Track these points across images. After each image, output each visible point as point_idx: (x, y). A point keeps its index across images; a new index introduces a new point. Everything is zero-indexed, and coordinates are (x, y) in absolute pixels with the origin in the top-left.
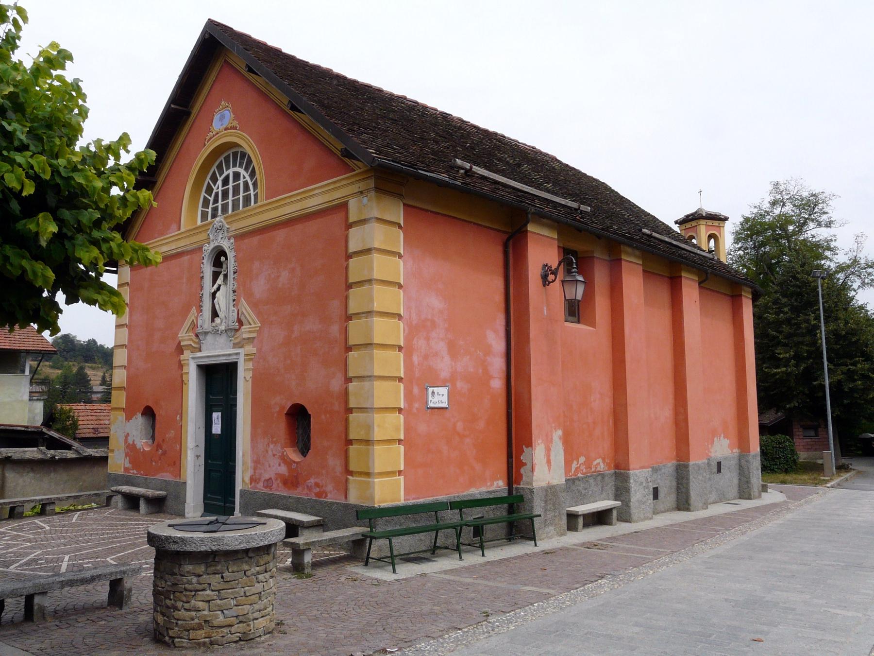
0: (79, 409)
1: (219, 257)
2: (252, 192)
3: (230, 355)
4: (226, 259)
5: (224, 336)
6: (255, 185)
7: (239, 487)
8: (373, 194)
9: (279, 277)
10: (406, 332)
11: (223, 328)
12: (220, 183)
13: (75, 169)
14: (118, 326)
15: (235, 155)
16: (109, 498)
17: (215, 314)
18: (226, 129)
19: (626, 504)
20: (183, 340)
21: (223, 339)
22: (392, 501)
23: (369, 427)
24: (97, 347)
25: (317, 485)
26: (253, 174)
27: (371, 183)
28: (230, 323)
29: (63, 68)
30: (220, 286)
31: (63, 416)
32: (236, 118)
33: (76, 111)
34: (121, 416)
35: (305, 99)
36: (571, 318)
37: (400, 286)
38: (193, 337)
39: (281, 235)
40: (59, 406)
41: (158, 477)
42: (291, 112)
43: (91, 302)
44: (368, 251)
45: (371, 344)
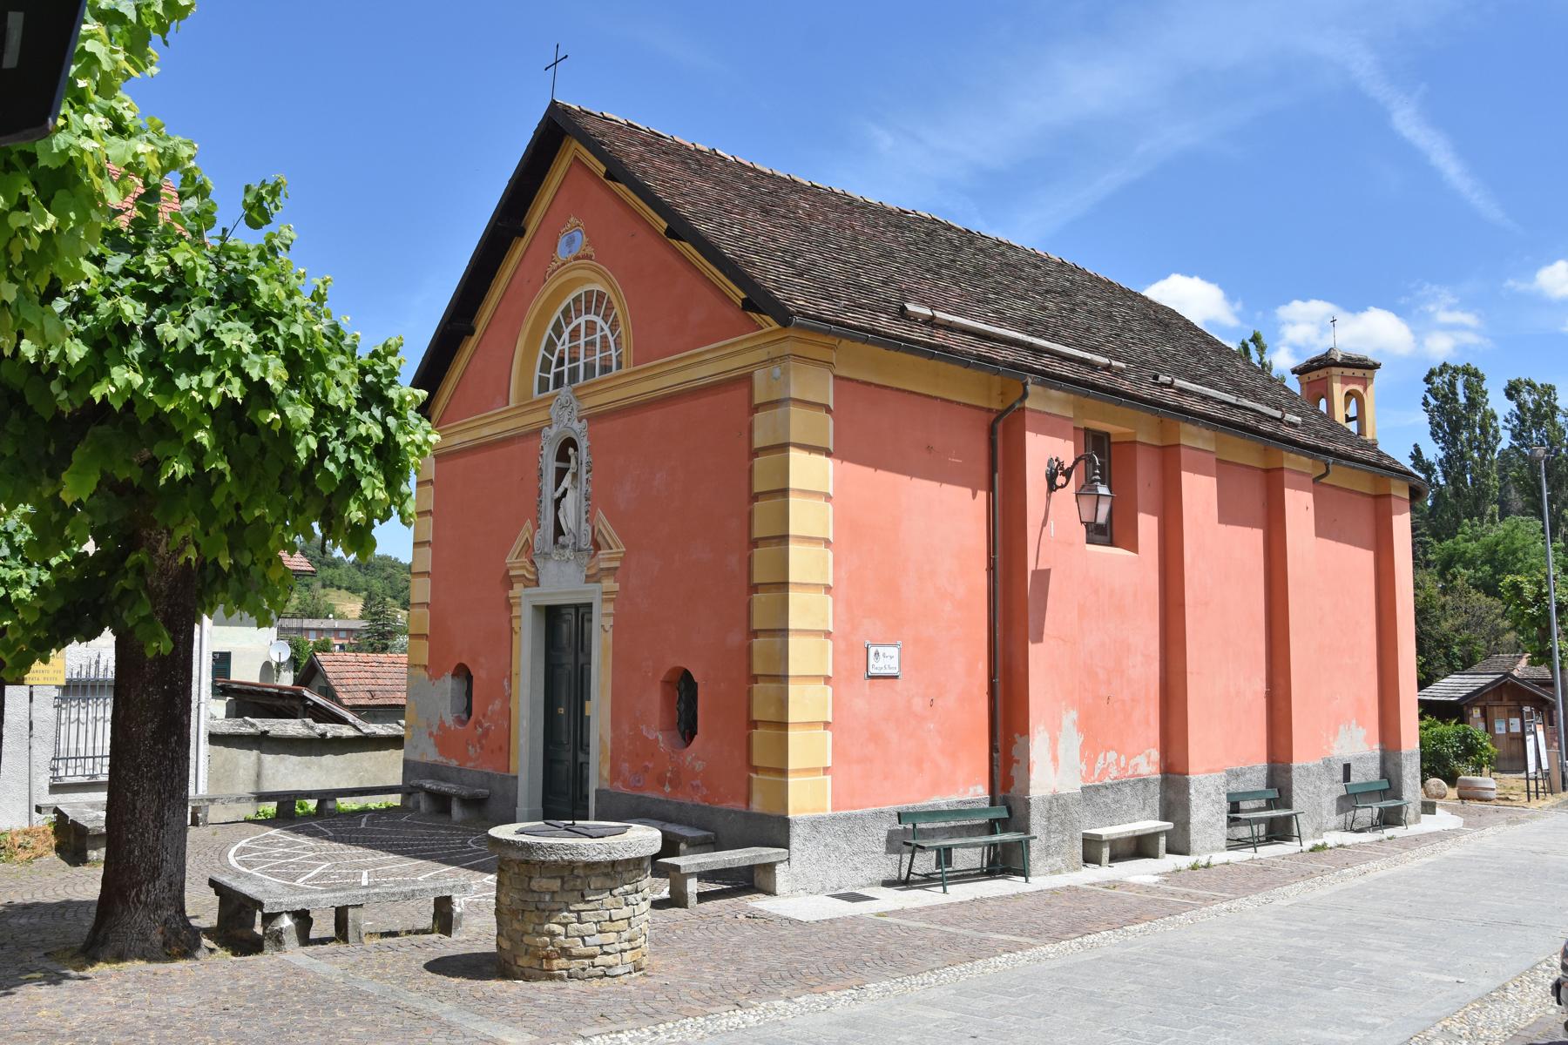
12: (566, 336)
17: (559, 531)
18: (577, 258)
19: (1183, 826)
22: (814, 810)
26: (614, 327)
32: (591, 243)
36: (1098, 537)
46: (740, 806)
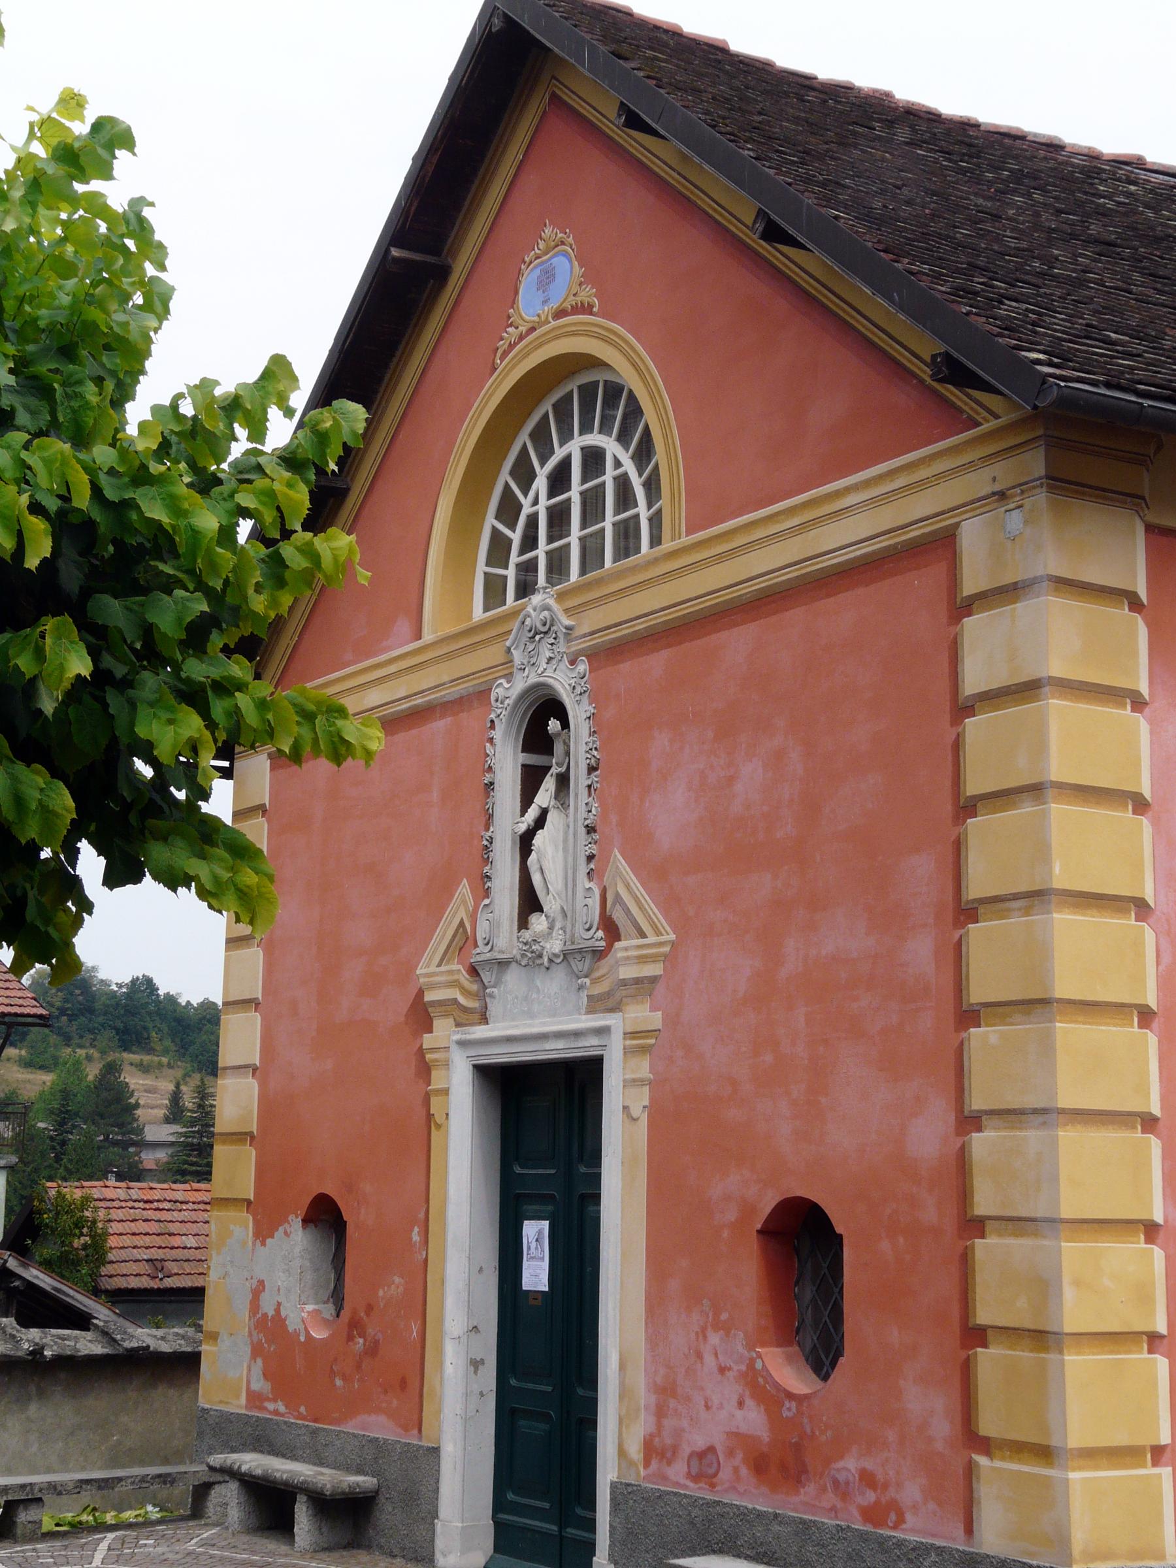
0: (108, 1198)
1: (542, 718)
2: (642, 510)
3: (577, 1034)
4: (565, 725)
5: (559, 976)
6: (652, 486)
7: (607, 1473)
8: (1041, 498)
9: (731, 780)
10: (1166, 959)
11: (554, 946)
12: (541, 484)
13: (141, 477)
14: (233, 942)
15: (588, 392)
16: (202, 1491)
17: (530, 902)
18: (560, 313)
20: (433, 987)
21: (554, 984)
23: (1045, 1287)
24: (158, 1002)
25: (868, 1479)
26: (644, 454)
27: (1035, 463)
28: (580, 931)
29: (107, 175)
30: (544, 813)
31: (66, 1221)
33: (138, 299)
34: (241, 1225)
35: (809, 200)
37: (1140, 805)
38: (464, 977)
39: (737, 643)
40: (52, 1188)
41: (350, 1427)
42: (764, 247)
43: (173, 880)
44: (1028, 690)
45: (1045, 1002)
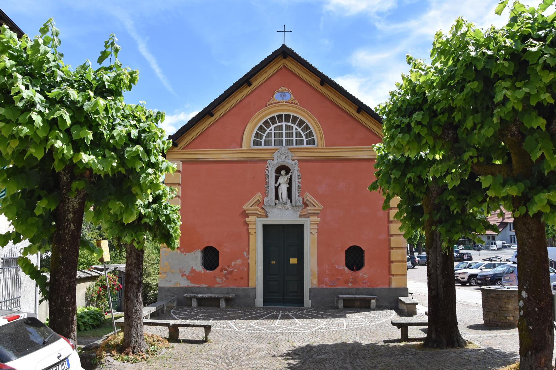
18: (287, 102)
46: (387, 286)
